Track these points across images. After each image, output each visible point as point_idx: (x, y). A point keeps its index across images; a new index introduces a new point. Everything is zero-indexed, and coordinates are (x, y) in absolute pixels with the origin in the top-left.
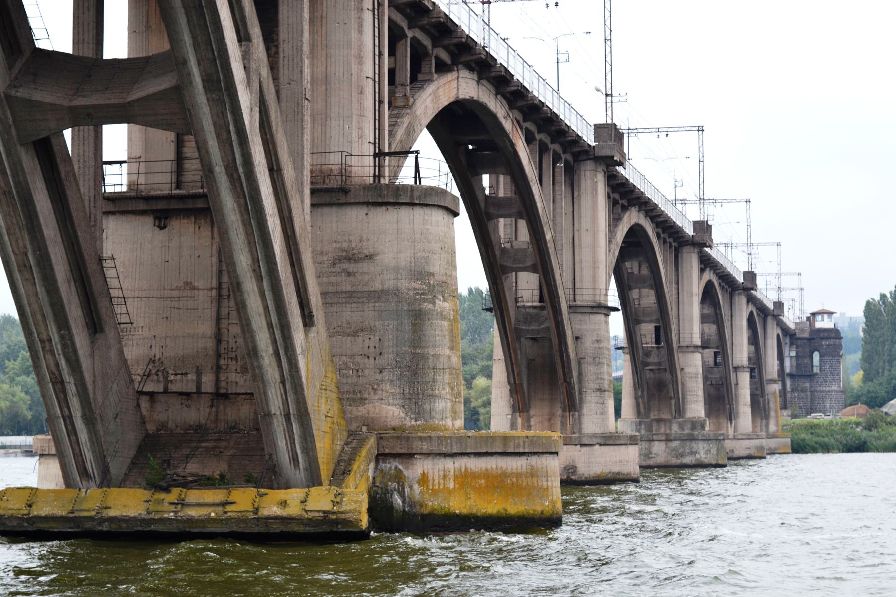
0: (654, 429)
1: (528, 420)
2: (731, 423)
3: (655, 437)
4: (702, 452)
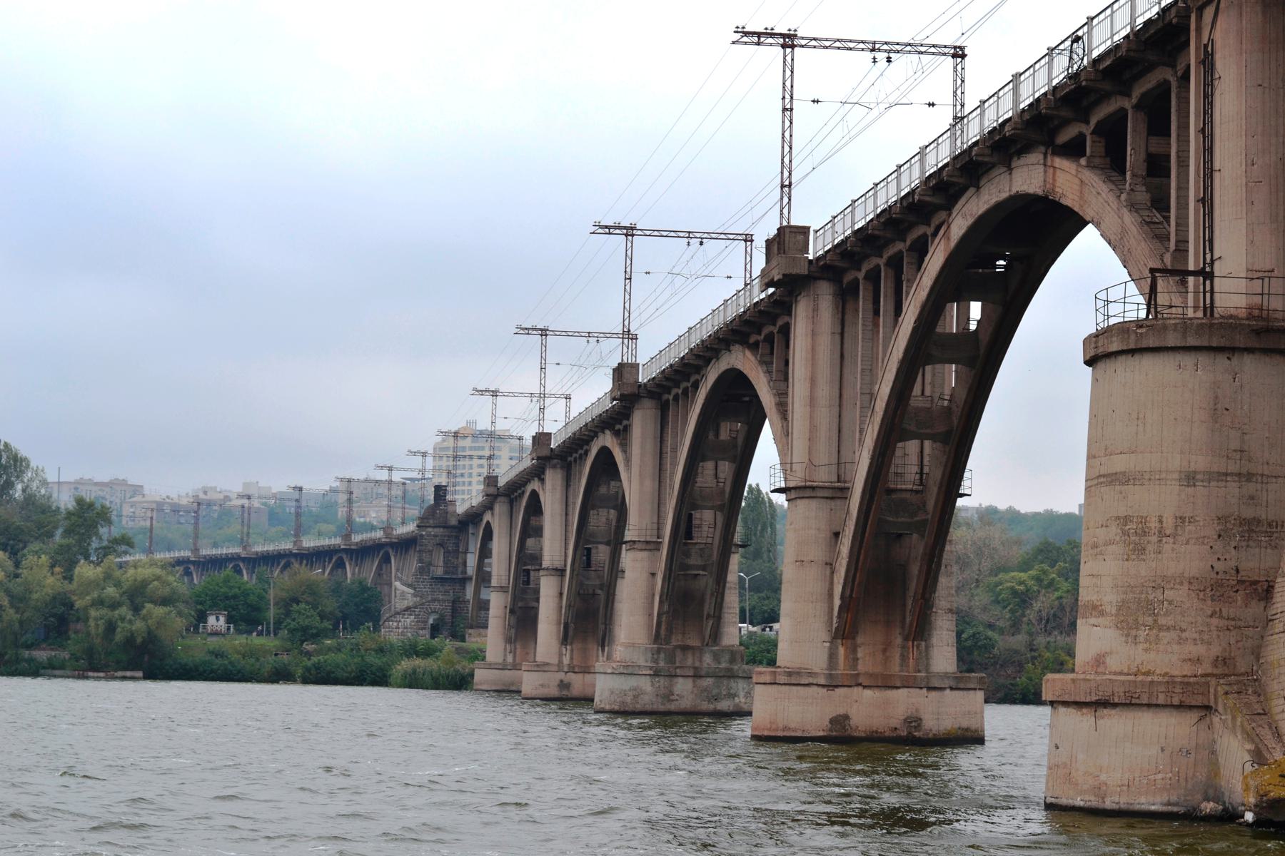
0: (678, 659)
1: (854, 651)
2: (603, 650)
3: (679, 672)
4: (742, 694)
